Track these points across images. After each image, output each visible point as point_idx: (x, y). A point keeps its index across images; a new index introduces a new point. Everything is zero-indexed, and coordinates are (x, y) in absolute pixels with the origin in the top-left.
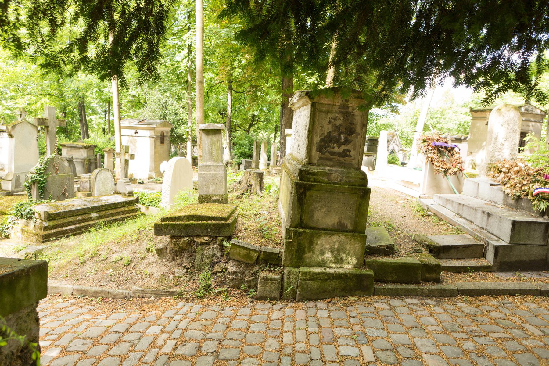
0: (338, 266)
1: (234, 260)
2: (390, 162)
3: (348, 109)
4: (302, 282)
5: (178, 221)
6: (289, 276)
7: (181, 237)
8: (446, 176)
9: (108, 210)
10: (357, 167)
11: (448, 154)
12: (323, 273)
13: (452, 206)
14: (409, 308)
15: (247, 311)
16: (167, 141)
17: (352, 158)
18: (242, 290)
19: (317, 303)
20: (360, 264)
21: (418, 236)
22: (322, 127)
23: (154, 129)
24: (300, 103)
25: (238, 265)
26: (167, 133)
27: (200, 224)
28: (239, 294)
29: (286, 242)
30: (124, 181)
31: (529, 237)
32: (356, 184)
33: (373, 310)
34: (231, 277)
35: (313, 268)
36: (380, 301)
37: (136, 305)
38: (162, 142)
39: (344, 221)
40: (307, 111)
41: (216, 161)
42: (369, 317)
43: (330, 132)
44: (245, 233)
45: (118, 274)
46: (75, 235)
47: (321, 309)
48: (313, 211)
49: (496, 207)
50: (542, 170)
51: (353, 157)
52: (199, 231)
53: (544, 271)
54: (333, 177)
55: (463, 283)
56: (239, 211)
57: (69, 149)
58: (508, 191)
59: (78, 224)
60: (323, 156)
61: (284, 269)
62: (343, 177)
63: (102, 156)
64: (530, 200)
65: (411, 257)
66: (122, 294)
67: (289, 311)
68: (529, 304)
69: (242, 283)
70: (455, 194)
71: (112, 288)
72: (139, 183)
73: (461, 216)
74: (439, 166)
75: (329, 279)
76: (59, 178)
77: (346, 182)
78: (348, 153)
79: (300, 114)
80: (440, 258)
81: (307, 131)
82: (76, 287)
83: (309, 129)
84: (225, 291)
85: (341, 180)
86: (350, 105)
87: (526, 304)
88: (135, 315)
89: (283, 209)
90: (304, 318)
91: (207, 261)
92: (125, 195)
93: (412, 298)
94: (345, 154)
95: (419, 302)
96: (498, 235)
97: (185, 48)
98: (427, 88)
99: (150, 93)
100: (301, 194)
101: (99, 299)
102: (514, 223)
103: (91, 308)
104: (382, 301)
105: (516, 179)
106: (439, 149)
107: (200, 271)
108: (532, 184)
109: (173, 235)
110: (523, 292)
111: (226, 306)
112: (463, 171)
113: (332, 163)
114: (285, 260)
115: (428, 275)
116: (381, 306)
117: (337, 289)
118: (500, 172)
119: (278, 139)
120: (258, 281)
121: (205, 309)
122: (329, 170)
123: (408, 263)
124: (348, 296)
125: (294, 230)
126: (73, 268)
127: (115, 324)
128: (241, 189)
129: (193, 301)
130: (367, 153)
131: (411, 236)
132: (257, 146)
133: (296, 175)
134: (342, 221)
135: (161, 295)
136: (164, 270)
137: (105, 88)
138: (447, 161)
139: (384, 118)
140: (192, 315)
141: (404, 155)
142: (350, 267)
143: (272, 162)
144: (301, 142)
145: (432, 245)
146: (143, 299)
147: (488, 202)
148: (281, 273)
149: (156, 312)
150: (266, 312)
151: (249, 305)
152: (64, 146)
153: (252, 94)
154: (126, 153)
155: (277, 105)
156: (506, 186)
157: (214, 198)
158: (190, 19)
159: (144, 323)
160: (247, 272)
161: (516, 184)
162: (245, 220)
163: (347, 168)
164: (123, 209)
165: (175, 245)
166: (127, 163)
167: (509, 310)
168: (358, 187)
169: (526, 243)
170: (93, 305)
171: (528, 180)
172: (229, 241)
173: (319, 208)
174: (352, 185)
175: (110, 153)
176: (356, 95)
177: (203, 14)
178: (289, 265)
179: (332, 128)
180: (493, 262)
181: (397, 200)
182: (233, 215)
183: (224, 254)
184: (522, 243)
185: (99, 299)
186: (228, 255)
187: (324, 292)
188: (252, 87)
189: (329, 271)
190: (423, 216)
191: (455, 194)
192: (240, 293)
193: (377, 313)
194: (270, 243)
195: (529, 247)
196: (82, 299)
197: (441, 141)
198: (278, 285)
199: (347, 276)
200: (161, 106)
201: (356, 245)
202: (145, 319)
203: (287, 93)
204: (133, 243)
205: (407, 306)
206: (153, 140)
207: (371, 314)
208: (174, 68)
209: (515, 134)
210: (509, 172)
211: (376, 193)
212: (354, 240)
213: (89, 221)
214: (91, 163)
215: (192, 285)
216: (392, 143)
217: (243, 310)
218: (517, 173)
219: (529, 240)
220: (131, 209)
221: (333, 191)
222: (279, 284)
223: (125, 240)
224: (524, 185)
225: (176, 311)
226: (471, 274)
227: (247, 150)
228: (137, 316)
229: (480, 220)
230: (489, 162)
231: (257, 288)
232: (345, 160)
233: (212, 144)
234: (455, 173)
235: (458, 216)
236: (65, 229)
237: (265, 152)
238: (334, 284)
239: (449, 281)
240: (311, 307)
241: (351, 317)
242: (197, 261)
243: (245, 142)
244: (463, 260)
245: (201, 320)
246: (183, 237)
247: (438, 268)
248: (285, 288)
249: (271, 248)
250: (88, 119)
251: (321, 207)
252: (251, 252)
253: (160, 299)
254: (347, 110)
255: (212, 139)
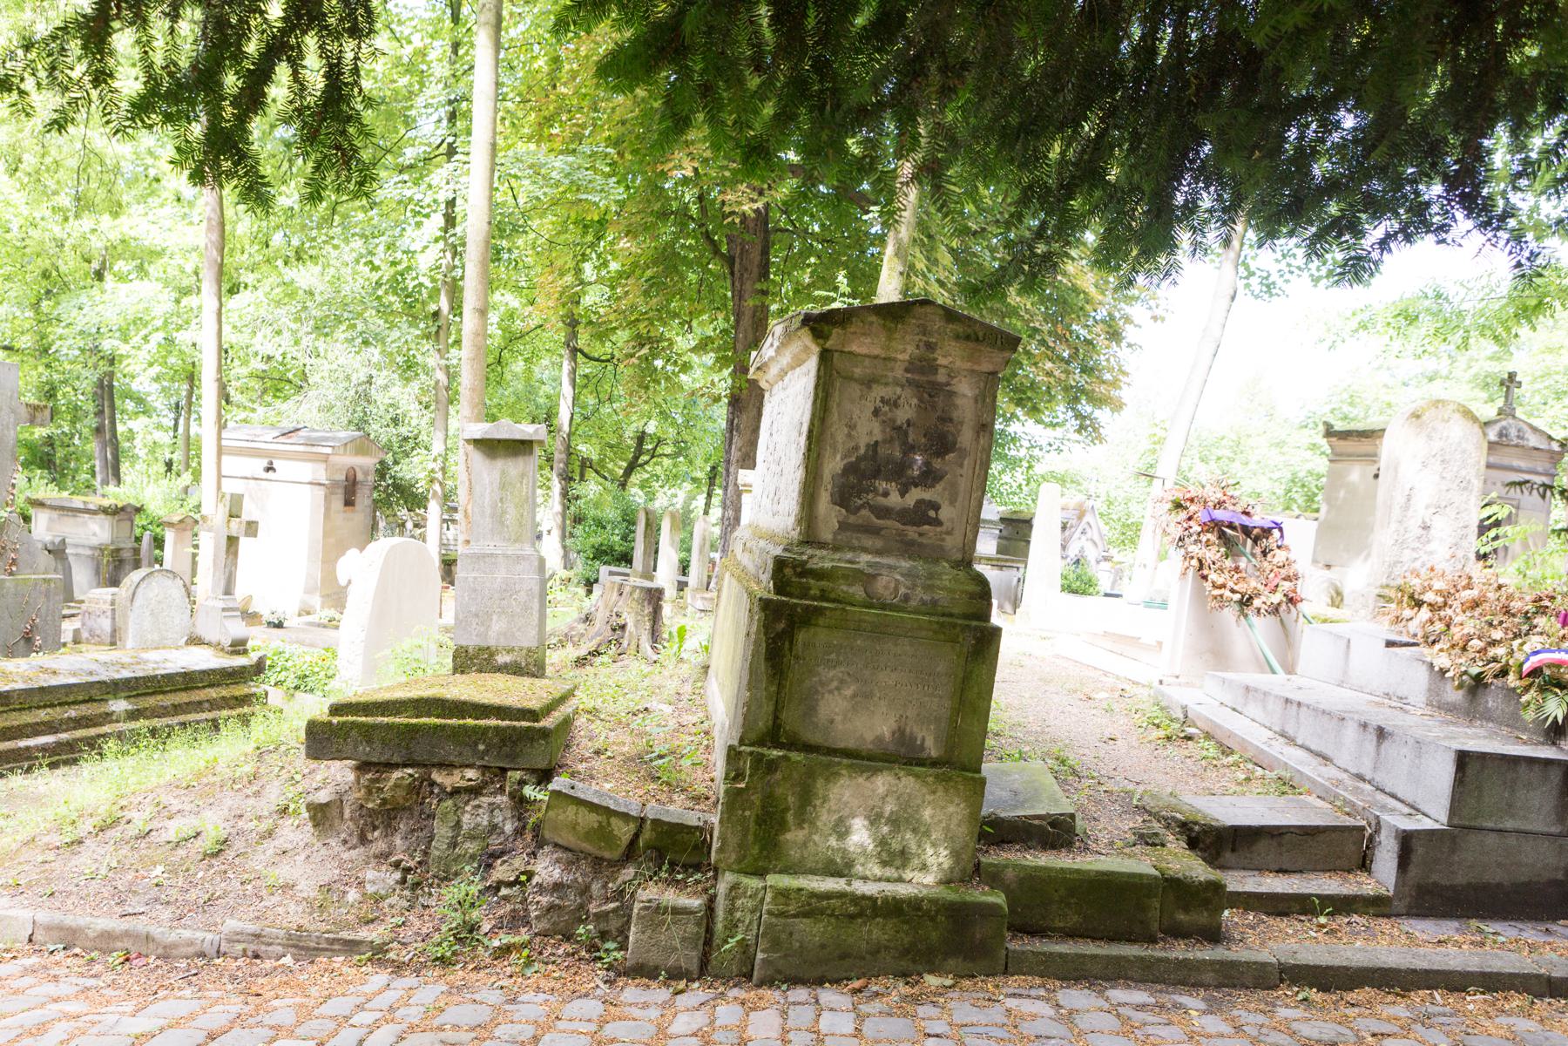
0: (890, 872)
1: (556, 845)
2: (1070, 589)
3: (936, 373)
4: (774, 920)
5: (383, 715)
6: (733, 900)
7: (391, 766)
8: (1246, 616)
9: (164, 693)
10: (959, 556)
11: (1253, 548)
12: (841, 895)
13: (1264, 707)
14: (1118, 1016)
15: (593, 1007)
16: (363, 499)
17: (944, 528)
18: (578, 942)
19: (819, 990)
20: (964, 870)
21: (1153, 796)
22: (852, 427)
23: (325, 459)
24: (785, 359)
25: (570, 863)
26: (366, 473)
27: (453, 727)
28: (568, 955)
29: (727, 792)
30: (222, 605)
31: (1510, 806)
32: (956, 611)
33: (1001, 1019)
34: (545, 900)
35: (810, 877)
36: (1025, 992)
37: (233, 978)
38: (349, 503)
39: (915, 729)
40: (804, 380)
41: (515, 541)
42: (989, 1038)
43: (877, 442)
44: (598, 764)
45: (181, 879)
46: (53, 766)
47: (831, 1010)
48: (817, 692)
49: (1406, 712)
50: (1552, 598)
51: (947, 525)
52: (450, 751)
53: (1561, 922)
54: (883, 586)
55: (1296, 947)
56: (582, 700)
57: (55, 514)
58: (1442, 661)
59: (66, 731)
60: (852, 519)
61: (715, 878)
62: (914, 586)
63: (159, 542)
64: (1514, 689)
65: (1130, 856)
66: (191, 943)
67: (727, 1013)
68: (1512, 1020)
69: (581, 921)
70: (1274, 672)
71: (159, 925)
72: (269, 623)
73: (1291, 741)
74: (1223, 586)
75: (861, 914)
76: (17, 585)
77: (924, 603)
78: (932, 513)
79: (782, 395)
80: (1222, 868)
81: (803, 440)
82: (43, 916)
83: (810, 431)
84: (524, 946)
85: (906, 598)
86: (942, 361)
87: (1503, 1020)
88: (227, 1007)
89: (721, 692)
90: (775, 1034)
91: (472, 847)
92: (222, 650)
93: (1129, 987)
94: (923, 515)
95: (1152, 1000)
96: (1410, 800)
97: (435, 211)
98: (1182, 256)
99: (321, 350)
100: (780, 636)
101: (116, 958)
102: (1464, 760)
103: (88, 985)
104: (1033, 992)
105: (1466, 624)
106: (1224, 533)
107: (446, 879)
108: (1519, 641)
109: (364, 758)
110: (1492, 983)
111: (521, 989)
112: (1299, 605)
113: (879, 543)
114: (721, 850)
115: (1181, 917)
116: (1027, 1006)
117: (886, 948)
118: (1419, 604)
119: (716, 512)
120: (630, 917)
121: (457, 998)
122: (870, 565)
123: (1118, 873)
124: (920, 975)
125: (751, 753)
126: (40, 859)
127: (162, 1030)
128: (592, 638)
129: (418, 972)
130: (998, 560)
131: (1130, 794)
132: (648, 524)
133: (766, 577)
134: (908, 730)
135: (317, 949)
136: (330, 873)
137: (182, 332)
138: (1250, 570)
139: (1054, 453)
140: (413, 1014)
141: (1116, 574)
142: (929, 879)
143: (693, 578)
144: (784, 478)
145: (1196, 823)
146: (258, 961)
147: (1377, 699)
148: (706, 890)
149: (298, 1000)
150: (654, 1013)
151: (598, 992)
152: (39, 504)
153: (639, 365)
154: (231, 516)
155: (717, 399)
156: (1437, 647)
157: (502, 659)
158: (454, 125)
159: (255, 1030)
160: (596, 887)
161: (1469, 638)
162: (597, 726)
163: (926, 560)
164: (213, 693)
165: (369, 792)
166: (232, 549)
167: (1447, 1034)
168: (960, 622)
169: (1501, 826)
170: (95, 976)
171: (1507, 629)
172: (542, 786)
173: (835, 684)
174: (943, 615)
175: (185, 530)
176: (960, 329)
177: (496, 111)
178: (734, 867)
179: (883, 431)
180: (1396, 886)
181: (1086, 690)
182: (562, 708)
183: (524, 827)
184: (1490, 825)
185: (116, 958)
186: (537, 828)
187: (844, 956)
188: (641, 341)
189: (860, 888)
190: (1169, 738)
191: (1274, 672)
192: (573, 954)
193: (1016, 1027)
194: (675, 797)
195: (1512, 841)
196: (60, 956)
197: (1231, 508)
198: (696, 929)
199: (919, 909)
200: (352, 392)
201: (951, 809)
202: (259, 1018)
203: (750, 329)
204: (236, 787)
205: (1114, 1009)
206: (321, 492)
207: (994, 1028)
208: (397, 273)
209: (1466, 493)
210: (1445, 604)
211: (1020, 670)
212: (946, 790)
213: (101, 725)
214: (121, 561)
215: (417, 923)
216: (1077, 534)
217: (578, 1003)
218: (1473, 608)
219: (1513, 816)
220: (237, 693)
221: (880, 631)
222: (698, 924)
223: (212, 779)
224: (1493, 643)
225: (362, 999)
226: (1323, 920)
227: (617, 539)
228: (235, 1009)
229: (1352, 750)
230: (1384, 581)
231: (627, 937)
232: (921, 535)
233: (503, 486)
234: (1275, 610)
235: (1282, 740)
236: (23, 743)
237: (672, 545)
238: (877, 932)
239: (1251, 937)
240: (799, 1003)
241: (929, 1035)
242: (439, 847)
243: (611, 513)
244: (1298, 876)
245: (441, 1029)
246: (396, 766)
247: (1214, 895)
248: (717, 941)
249: (677, 810)
250: (120, 428)
251: (842, 681)
252: (614, 820)
253: (312, 962)
254: (932, 378)
255: (503, 473)
